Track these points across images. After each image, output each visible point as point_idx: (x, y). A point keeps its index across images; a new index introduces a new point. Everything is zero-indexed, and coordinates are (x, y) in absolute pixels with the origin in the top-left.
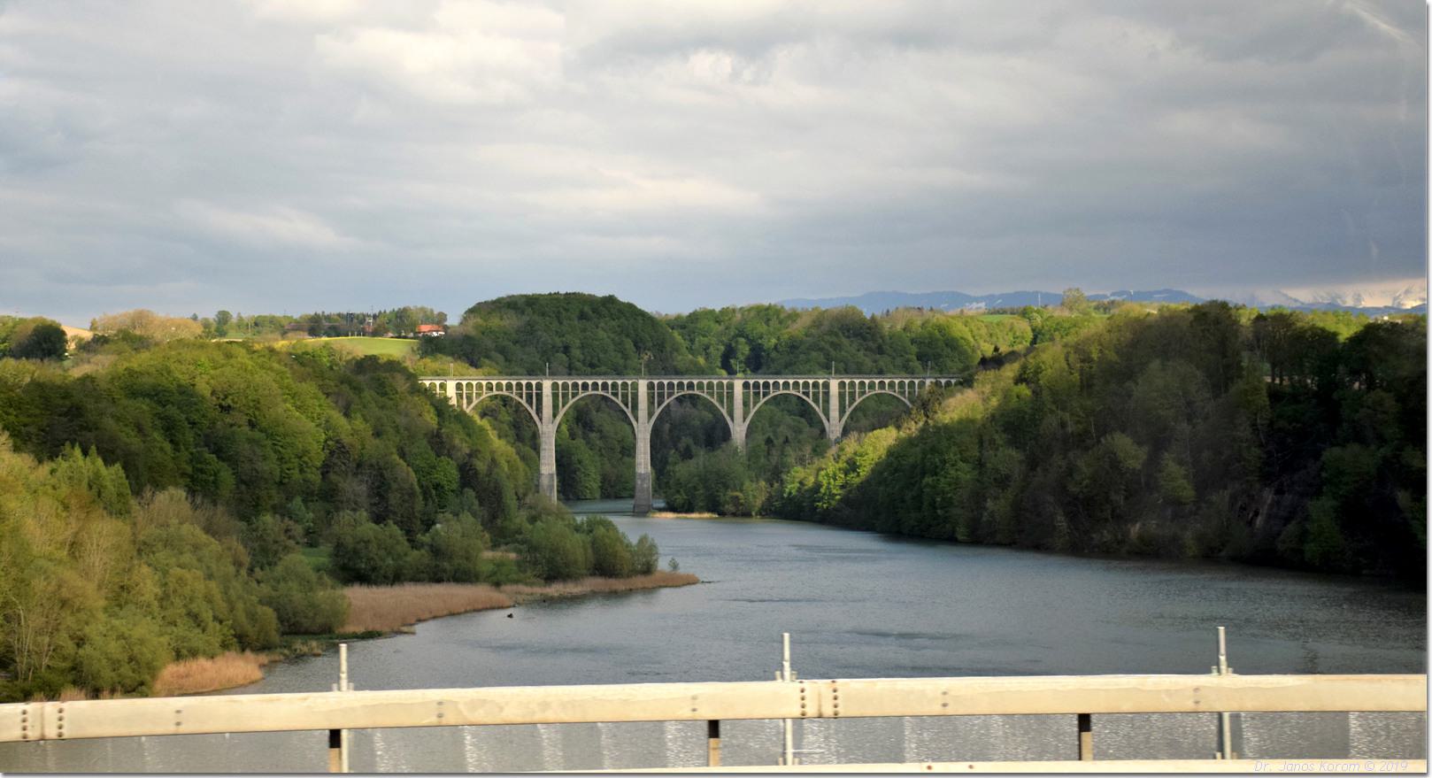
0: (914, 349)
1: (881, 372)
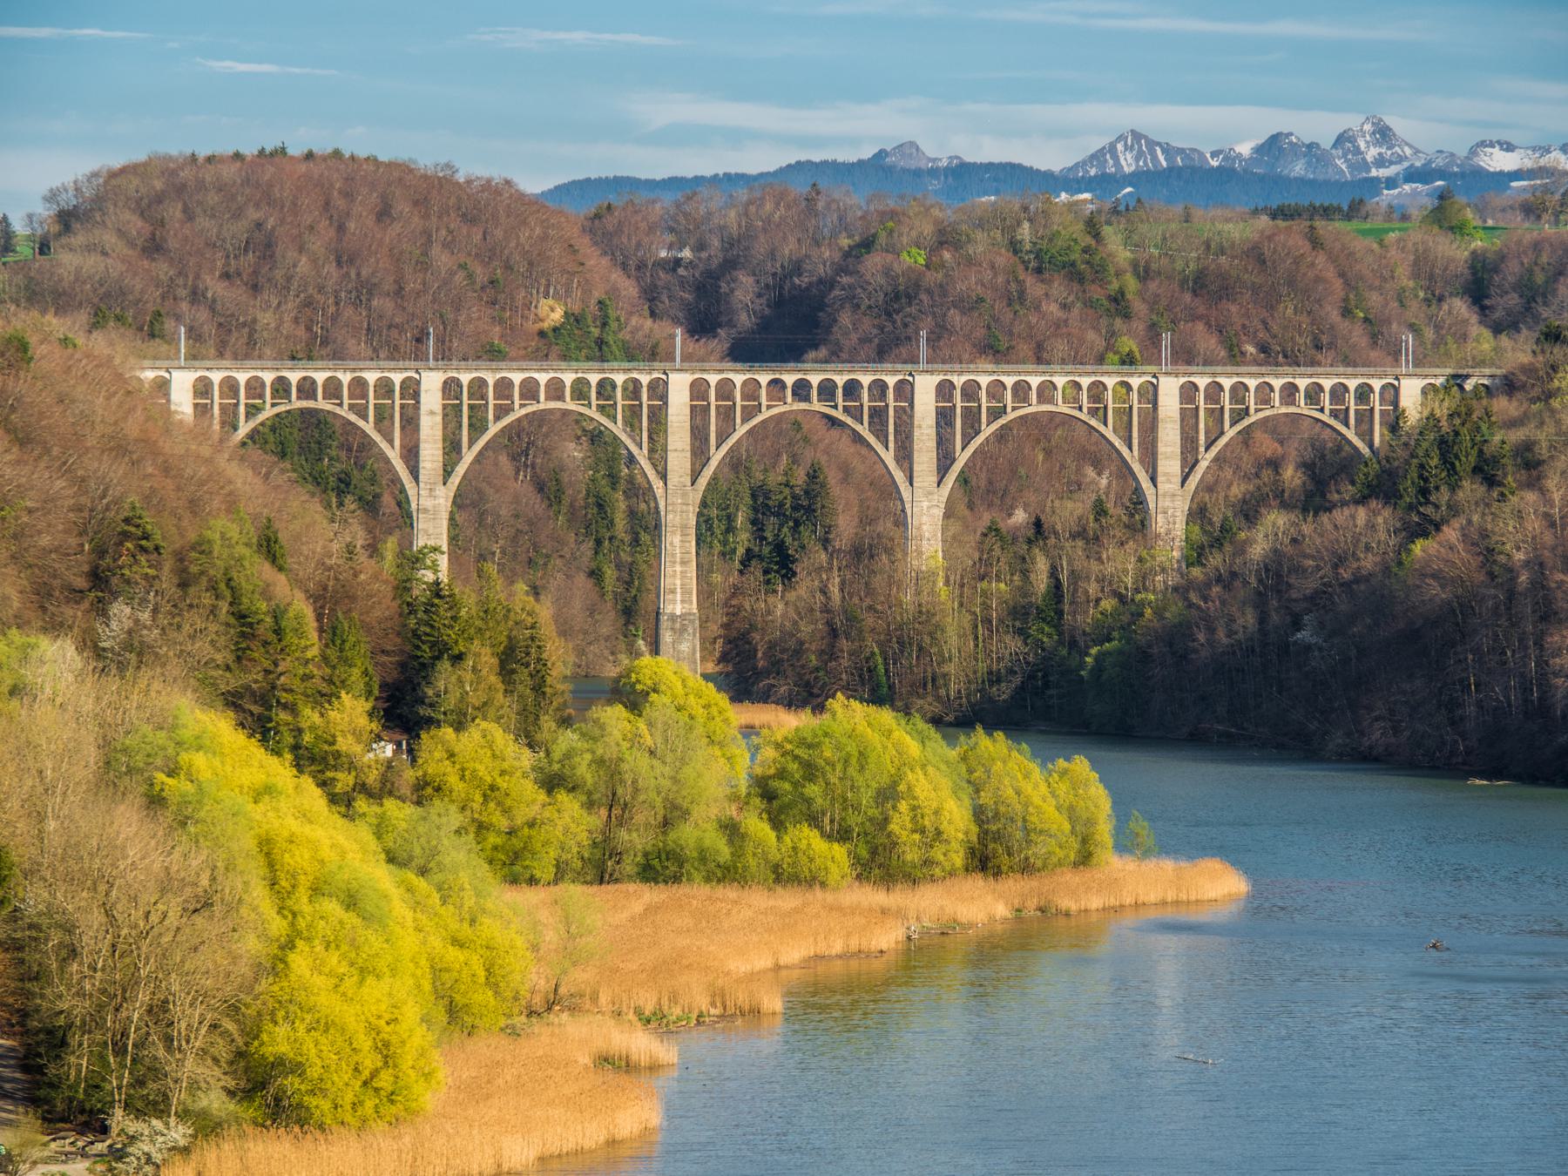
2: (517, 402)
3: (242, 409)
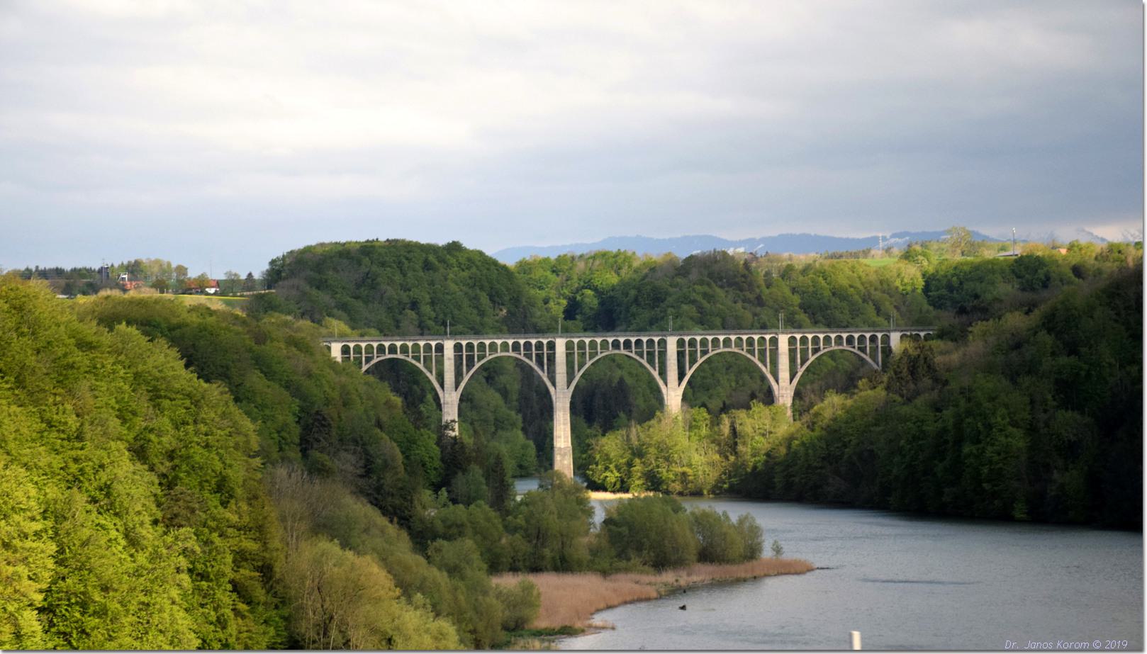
0: (796, 299)
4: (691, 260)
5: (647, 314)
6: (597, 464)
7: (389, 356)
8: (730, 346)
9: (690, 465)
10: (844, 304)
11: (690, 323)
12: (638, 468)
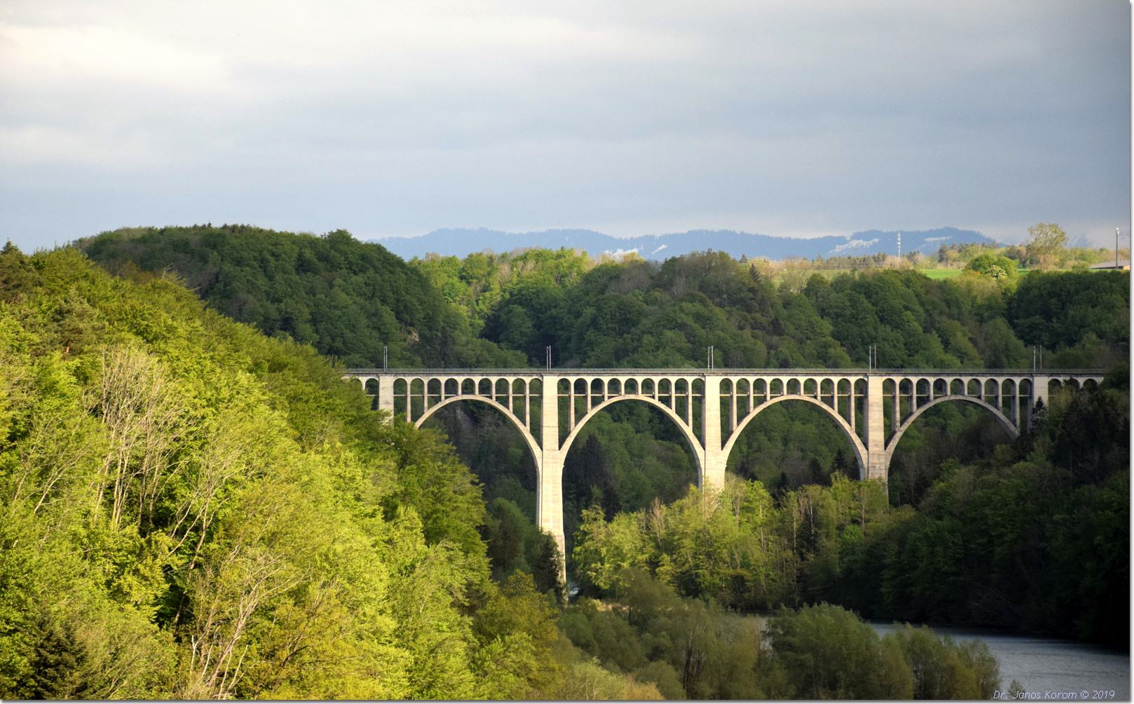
1: (784, 365)
2: (443, 396)
3: (915, 401)
4: (672, 265)
5: (610, 344)
6: (602, 561)
7: (461, 397)
8: (473, 392)
9: (746, 565)
10: (897, 334)
11: (678, 357)
12: (667, 566)
